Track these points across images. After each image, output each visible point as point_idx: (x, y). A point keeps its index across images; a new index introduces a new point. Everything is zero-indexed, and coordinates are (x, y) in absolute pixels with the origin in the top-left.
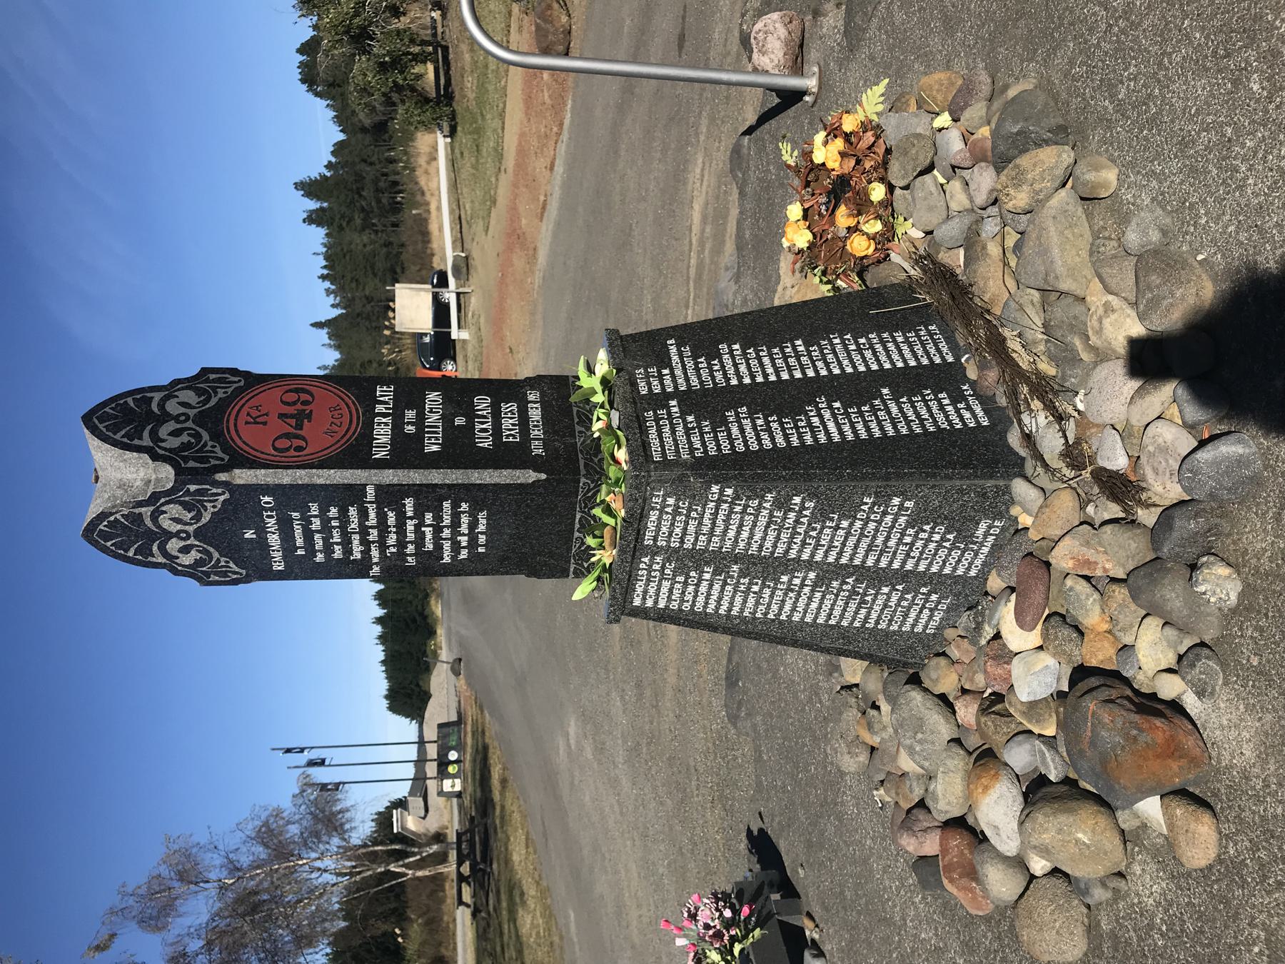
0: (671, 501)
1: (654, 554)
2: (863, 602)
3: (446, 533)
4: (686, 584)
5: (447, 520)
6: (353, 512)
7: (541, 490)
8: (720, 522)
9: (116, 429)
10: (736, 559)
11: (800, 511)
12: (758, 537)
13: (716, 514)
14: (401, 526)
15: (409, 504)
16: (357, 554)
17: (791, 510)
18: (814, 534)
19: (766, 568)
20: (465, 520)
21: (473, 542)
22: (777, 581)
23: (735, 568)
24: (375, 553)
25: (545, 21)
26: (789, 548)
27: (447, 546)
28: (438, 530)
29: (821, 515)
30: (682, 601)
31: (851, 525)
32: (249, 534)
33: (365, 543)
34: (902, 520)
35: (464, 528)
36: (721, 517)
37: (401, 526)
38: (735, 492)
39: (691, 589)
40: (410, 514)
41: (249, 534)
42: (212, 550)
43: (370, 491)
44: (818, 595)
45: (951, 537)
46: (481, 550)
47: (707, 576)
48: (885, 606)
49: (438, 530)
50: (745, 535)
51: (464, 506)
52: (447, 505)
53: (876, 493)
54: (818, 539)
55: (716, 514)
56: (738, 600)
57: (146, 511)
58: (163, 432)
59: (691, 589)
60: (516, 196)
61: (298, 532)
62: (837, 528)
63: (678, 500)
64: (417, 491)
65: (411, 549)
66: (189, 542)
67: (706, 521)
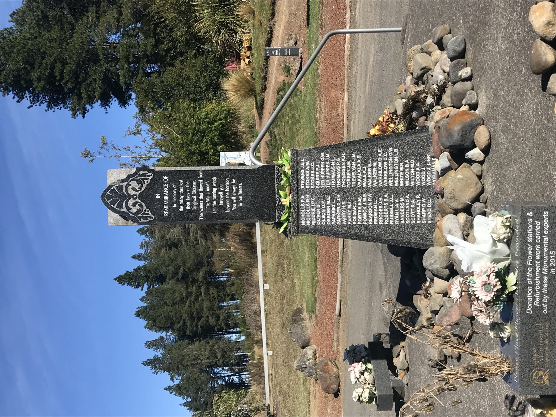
1: (306, 193)
2: (395, 208)
5: (228, 189)
6: (194, 184)
7: (261, 172)
8: (328, 172)
9: (113, 203)
10: (338, 191)
11: (356, 161)
13: (325, 168)
17: (353, 161)
18: (364, 172)
20: (234, 188)
23: (339, 196)
24: (202, 206)
25: (325, 372)
26: (357, 182)
27: (228, 201)
29: (365, 162)
31: (377, 164)
32: (158, 196)
34: (396, 158)
36: (328, 169)
37: (211, 191)
38: (330, 155)
40: (214, 185)
42: (143, 204)
43: (201, 173)
44: (375, 206)
45: (418, 165)
46: (241, 205)
47: (328, 203)
48: (405, 209)
50: (338, 177)
52: (227, 180)
53: (382, 147)
54: (367, 174)
55: (325, 168)
57: (124, 184)
62: (372, 167)
63: (310, 163)
66: (136, 200)
67: (323, 172)
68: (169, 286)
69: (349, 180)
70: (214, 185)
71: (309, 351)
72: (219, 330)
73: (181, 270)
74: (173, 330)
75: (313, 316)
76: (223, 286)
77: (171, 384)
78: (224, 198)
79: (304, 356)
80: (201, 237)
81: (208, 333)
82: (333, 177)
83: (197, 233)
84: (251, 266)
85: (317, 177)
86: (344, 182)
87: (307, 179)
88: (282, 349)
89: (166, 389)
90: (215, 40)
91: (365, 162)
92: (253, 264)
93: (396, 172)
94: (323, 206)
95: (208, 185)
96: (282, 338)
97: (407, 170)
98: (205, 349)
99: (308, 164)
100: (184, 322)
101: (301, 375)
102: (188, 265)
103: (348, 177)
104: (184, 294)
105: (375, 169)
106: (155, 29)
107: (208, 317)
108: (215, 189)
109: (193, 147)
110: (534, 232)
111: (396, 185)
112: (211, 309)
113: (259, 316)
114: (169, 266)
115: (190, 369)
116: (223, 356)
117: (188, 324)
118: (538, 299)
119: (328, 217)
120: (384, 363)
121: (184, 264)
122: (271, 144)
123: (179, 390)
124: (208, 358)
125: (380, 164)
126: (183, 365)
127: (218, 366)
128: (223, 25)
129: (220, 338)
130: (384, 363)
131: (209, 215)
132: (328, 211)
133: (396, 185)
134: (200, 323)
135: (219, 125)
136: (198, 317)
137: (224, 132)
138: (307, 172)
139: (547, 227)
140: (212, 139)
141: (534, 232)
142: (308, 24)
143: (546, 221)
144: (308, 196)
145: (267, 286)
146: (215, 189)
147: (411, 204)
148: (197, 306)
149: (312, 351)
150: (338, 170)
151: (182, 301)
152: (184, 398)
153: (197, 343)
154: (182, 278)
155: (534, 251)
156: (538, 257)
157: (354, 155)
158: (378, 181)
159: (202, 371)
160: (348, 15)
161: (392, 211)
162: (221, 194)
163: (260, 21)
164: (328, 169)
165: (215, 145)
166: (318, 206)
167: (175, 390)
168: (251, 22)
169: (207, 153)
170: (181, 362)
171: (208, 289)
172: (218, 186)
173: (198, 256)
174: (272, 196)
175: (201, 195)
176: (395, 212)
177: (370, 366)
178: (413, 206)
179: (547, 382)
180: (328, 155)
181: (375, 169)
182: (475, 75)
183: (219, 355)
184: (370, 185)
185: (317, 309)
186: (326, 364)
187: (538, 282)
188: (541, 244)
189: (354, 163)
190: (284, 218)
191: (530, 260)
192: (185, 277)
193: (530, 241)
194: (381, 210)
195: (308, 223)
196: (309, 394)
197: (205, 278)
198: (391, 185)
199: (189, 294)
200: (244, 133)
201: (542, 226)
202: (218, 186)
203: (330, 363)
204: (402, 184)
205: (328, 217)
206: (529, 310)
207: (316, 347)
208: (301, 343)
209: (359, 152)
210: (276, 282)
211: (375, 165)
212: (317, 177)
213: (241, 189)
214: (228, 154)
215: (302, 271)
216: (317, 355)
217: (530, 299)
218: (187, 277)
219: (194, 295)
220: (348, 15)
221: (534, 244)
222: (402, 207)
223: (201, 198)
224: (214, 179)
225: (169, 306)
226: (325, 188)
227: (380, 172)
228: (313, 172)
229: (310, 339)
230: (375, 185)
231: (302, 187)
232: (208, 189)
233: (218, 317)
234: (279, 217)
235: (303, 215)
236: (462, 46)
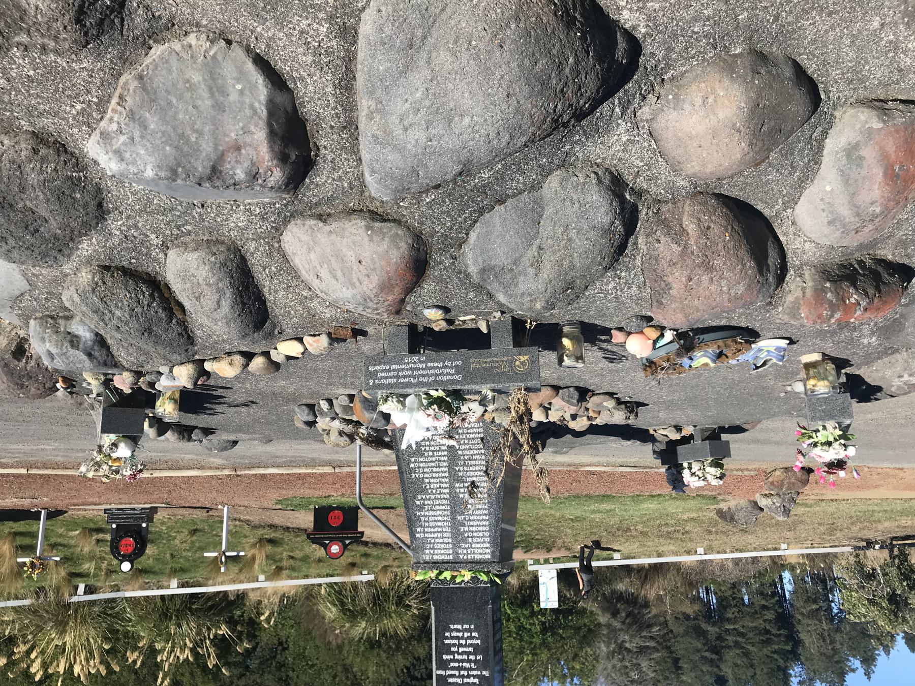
0: (427, 552)
1: (457, 553)
2: (469, 459)
5: (456, 642)
8: (435, 530)
10: (454, 519)
12: (440, 513)
20: (454, 634)
23: (459, 518)
24: (475, 673)
25: (782, 485)
27: (469, 642)
29: (424, 491)
30: (484, 536)
34: (421, 459)
35: (460, 634)
36: (432, 530)
37: (458, 661)
40: (452, 657)
43: (439, 672)
46: (472, 627)
47: (466, 529)
48: (470, 449)
50: (440, 518)
51: (447, 634)
52: (446, 642)
54: (437, 489)
60: (589, 497)
62: (430, 483)
64: (439, 654)
65: (472, 657)
67: (435, 535)
68: (730, 671)
69: (443, 508)
70: (452, 657)
71: (763, 502)
72: (781, 606)
73: (707, 654)
74: (786, 668)
75: (720, 497)
76: (722, 600)
77: (861, 671)
78: (466, 646)
79: (770, 508)
80: (650, 632)
81: (785, 621)
82: (440, 524)
83: (645, 637)
84: (679, 570)
85: (441, 541)
86: (445, 513)
87: (442, 553)
88: (774, 533)
89: (869, 678)
90: (416, 612)
91: (424, 491)
92: (677, 566)
93: (434, 459)
94: (470, 534)
95: (452, 664)
96: (759, 532)
97: (432, 448)
98: (808, 625)
99: (427, 552)
100: (775, 652)
101: (797, 510)
102: (700, 646)
103: (440, 508)
104: (737, 652)
105: (432, 481)
106: (416, 679)
107: (765, 621)
108: (457, 657)
109: (537, 641)
110: (387, 378)
111: (446, 458)
112: (754, 615)
113: (740, 559)
114: (702, 671)
115: (838, 646)
116: (815, 601)
117: (776, 647)
118: (448, 371)
119: (481, 529)
120: (680, 449)
121: (698, 651)
122: (526, 547)
123: (869, 661)
124: (820, 621)
125: (426, 475)
126: (833, 655)
127: (831, 609)
128: (400, 601)
129: (792, 605)
130: (680, 449)
131: (481, 666)
132: (474, 529)
133: (446, 458)
134: (774, 631)
135: (510, 608)
136: (767, 634)
137: (519, 602)
138: (436, 552)
139: (383, 367)
140: (527, 618)
141: (387, 378)
142: (392, 508)
143: (378, 368)
144: (460, 551)
145: (700, 550)
146: (457, 657)
147: (464, 444)
148: (751, 635)
149: (764, 499)
150: (433, 518)
151: (746, 654)
152: (879, 655)
153: (802, 636)
154: (716, 654)
155: (404, 377)
156: (410, 373)
157: (418, 503)
158: (443, 477)
159: (838, 630)
160: (377, 468)
161: (472, 463)
162: (461, 650)
163: (394, 559)
164: (432, 530)
165: (533, 614)
166: (470, 540)
167: (869, 666)
168: (395, 570)
169: (543, 623)
170: (829, 658)
171: (729, 620)
172: (453, 653)
173: (686, 633)
174: (463, 590)
175: (462, 672)
176: (473, 460)
177: (685, 465)
178: (466, 442)
179: (526, 357)
180: (418, 530)
181: (432, 481)
182: (326, 396)
183: (814, 607)
184: (447, 485)
185: (710, 493)
186: (772, 483)
187: (432, 371)
188: (399, 370)
189: (426, 502)
190: (484, 578)
191: (412, 380)
192: (715, 650)
193: (395, 380)
194: (472, 474)
195: (488, 551)
196: (823, 500)
197: (714, 624)
198: (446, 464)
199: (737, 645)
200: (519, 579)
201: (382, 371)
202: (453, 653)
203: (771, 479)
204: (445, 453)
205: (481, 529)
206: (458, 377)
207: (758, 495)
208: (757, 512)
209: (415, 497)
210: (691, 540)
211: (427, 481)
212: (441, 541)
213: (456, 626)
214: (542, 598)
215: (671, 510)
216: (767, 492)
217: (448, 377)
218: (715, 647)
219: (740, 639)
220: (377, 468)
221: (398, 377)
222: (468, 452)
223: (465, 673)
224: (445, 657)
225: (755, 673)
226: (452, 533)
227: (435, 475)
228: (436, 546)
229: (750, 501)
230: (447, 480)
231: (451, 557)
232: (456, 665)
233: (764, 607)
234: (485, 583)
235: (480, 557)
236: (304, 407)
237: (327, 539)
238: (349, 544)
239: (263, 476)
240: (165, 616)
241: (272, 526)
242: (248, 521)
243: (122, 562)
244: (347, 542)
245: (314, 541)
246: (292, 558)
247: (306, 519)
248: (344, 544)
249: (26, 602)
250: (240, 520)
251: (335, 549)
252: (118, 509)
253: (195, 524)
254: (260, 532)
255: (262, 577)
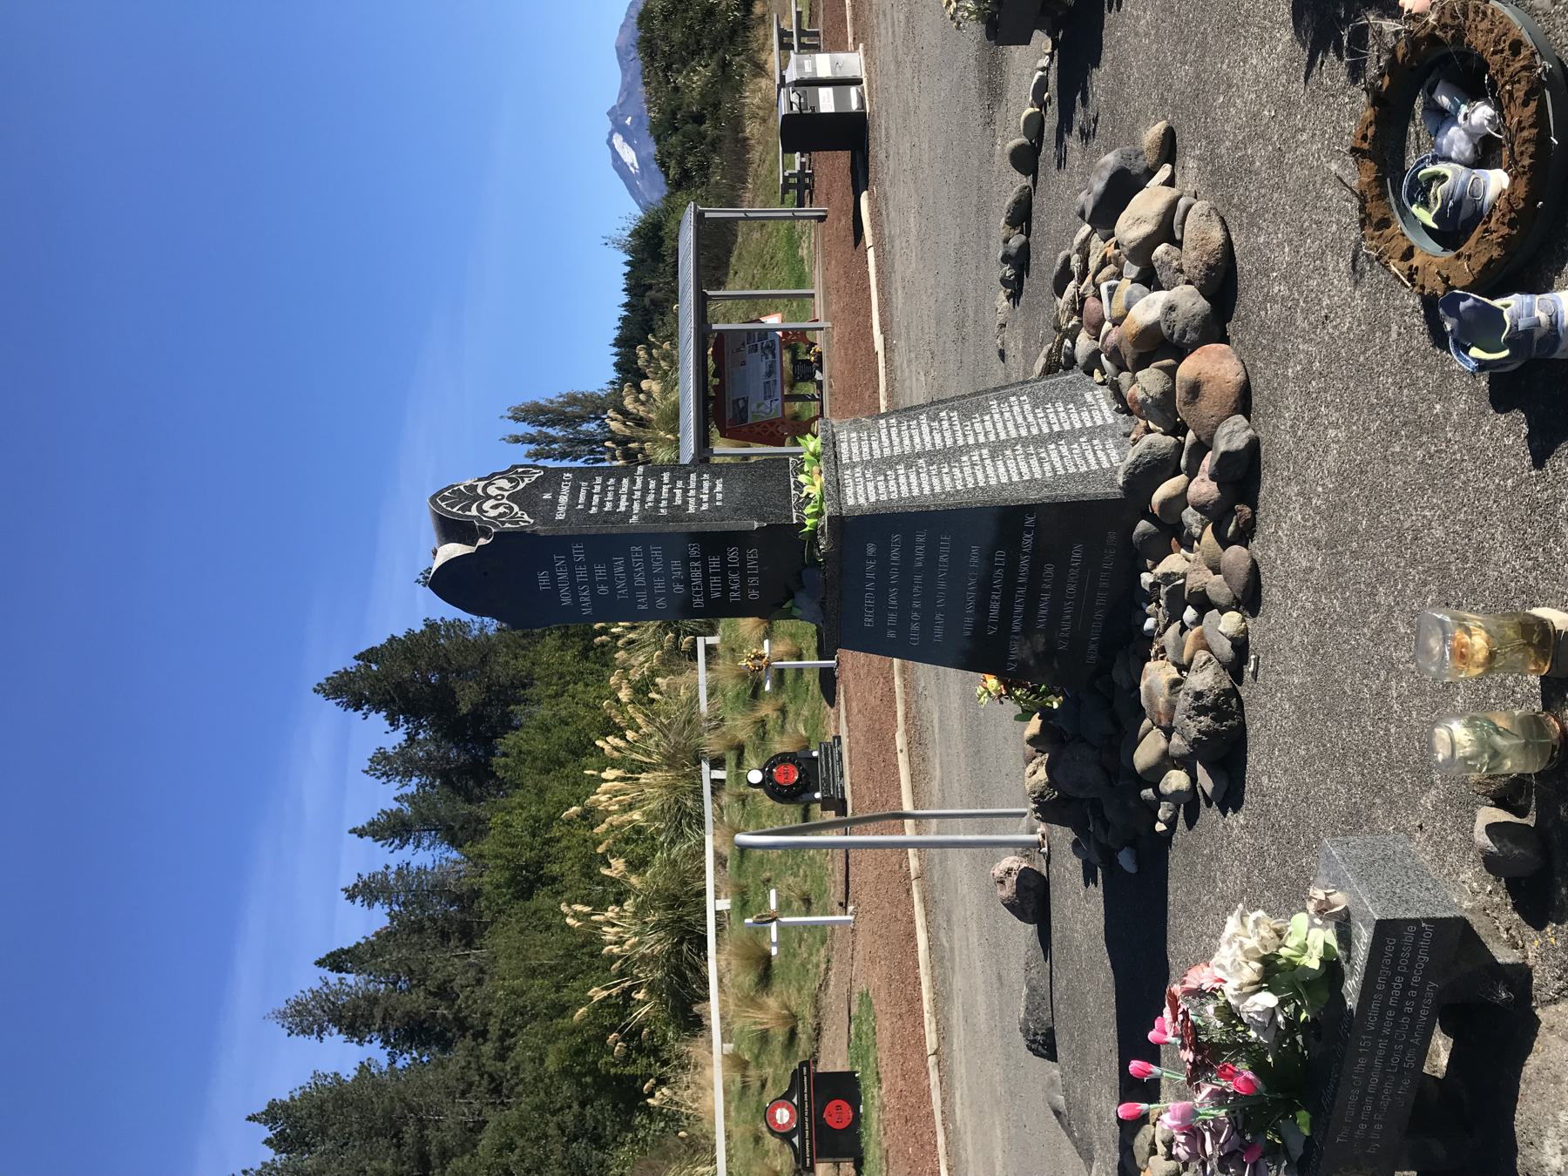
3: (692, 493)
4: (886, 480)
10: (919, 456)
14: (658, 490)
15: (666, 477)
16: (622, 508)
19: (949, 455)
20: (706, 485)
21: (712, 498)
22: (960, 461)
24: (636, 506)
27: (692, 501)
28: (685, 491)
33: (630, 500)
37: (658, 490)
39: (892, 483)
41: (547, 496)
49: (685, 491)
56: (936, 481)
58: (486, 506)
59: (892, 483)
61: (583, 493)
65: (664, 504)
237: (801, 1099)
238: (793, 1145)
239: (911, 936)
240: (673, 902)
241: (818, 1030)
242: (827, 985)
243: (762, 770)
244: (796, 1140)
245: (796, 1076)
246: (763, 1086)
247: (834, 1060)
248: (792, 1133)
249: (703, 706)
250: (828, 969)
251: (783, 1116)
252: (840, 754)
253: (820, 897)
254: (807, 1012)
255: (729, 1047)
